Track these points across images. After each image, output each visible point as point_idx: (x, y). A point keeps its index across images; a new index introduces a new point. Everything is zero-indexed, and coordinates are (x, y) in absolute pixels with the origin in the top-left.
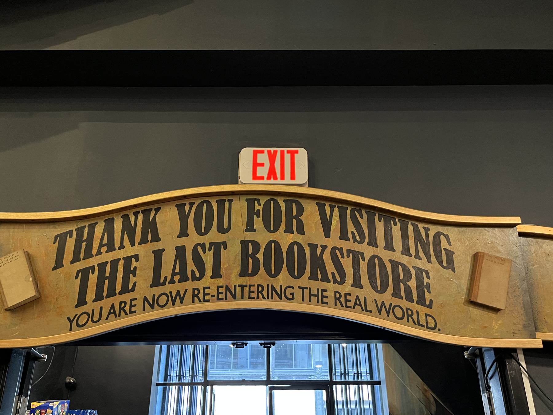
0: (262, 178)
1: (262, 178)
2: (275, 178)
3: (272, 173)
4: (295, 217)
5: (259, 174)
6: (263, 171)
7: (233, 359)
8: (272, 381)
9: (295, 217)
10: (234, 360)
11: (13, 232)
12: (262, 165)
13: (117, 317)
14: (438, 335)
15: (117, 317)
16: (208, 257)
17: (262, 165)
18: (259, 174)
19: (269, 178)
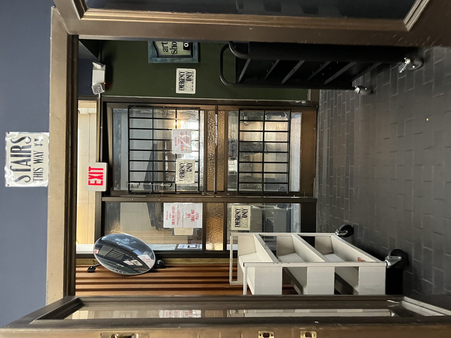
0: (102, 182)
1: (102, 182)
2: (102, 176)
3: (100, 178)
4: (21, 150)
5: (100, 183)
6: (99, 181)
7: (230, 263)
8: (77, 254)
9: (21, 150)
10: (229, 238)
11: (229, 206)
12: (96, 182)
13: (234, 251)
14: (53, 15)
15: (234, 251)
16: (156, 214)
17: (96, 182)
18: (100, 183)
19: (102, 179)
